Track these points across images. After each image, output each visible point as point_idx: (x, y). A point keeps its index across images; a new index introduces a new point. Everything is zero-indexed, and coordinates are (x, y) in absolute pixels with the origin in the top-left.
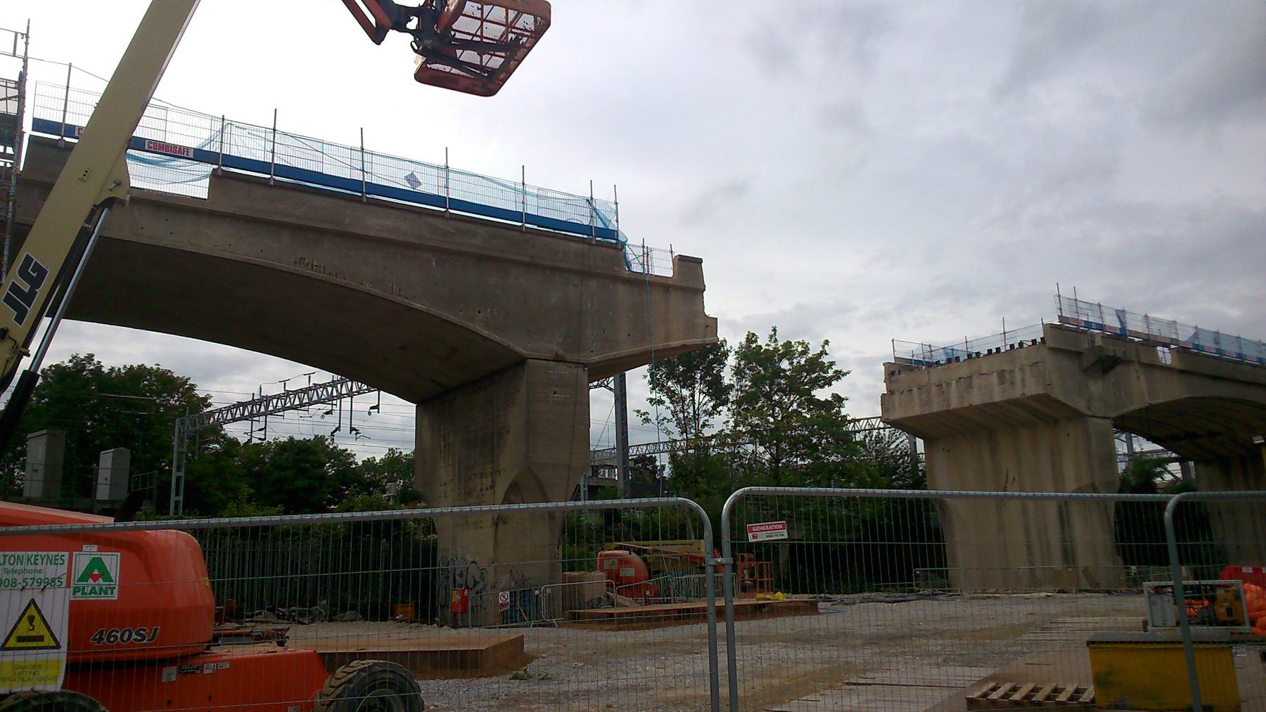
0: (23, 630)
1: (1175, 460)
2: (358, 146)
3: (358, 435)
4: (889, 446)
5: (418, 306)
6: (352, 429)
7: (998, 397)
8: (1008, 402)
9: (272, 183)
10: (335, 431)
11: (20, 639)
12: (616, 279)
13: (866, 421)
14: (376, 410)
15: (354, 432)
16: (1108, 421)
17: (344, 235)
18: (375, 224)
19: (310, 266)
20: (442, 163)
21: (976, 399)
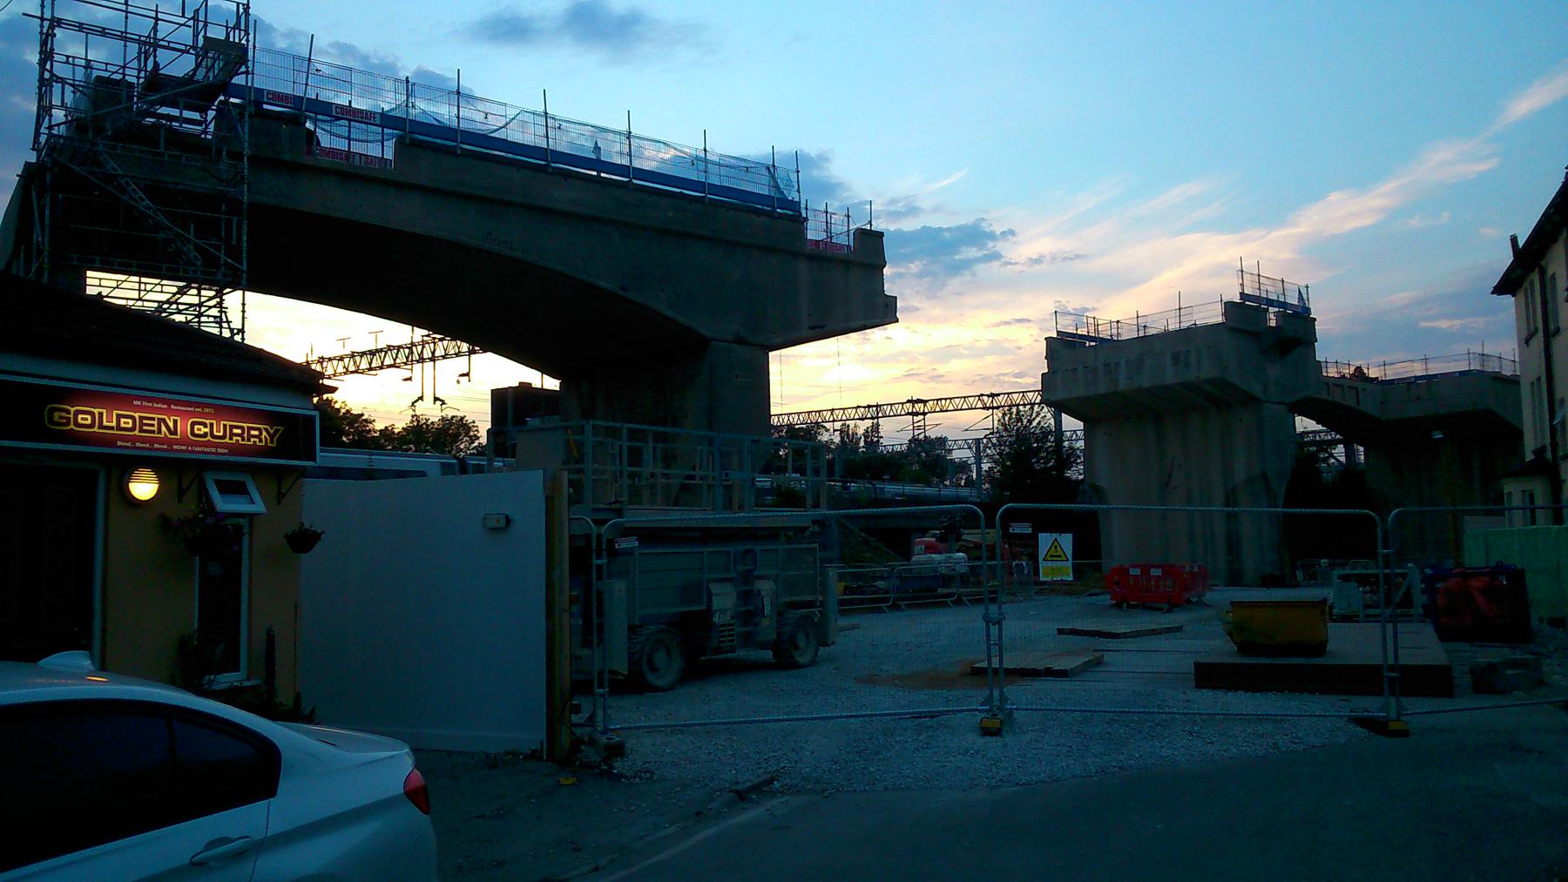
0: (1052, 551)
1: (1340, 442)
2: (541, 109)
3: (444, 406)
4: (1031, 424)
5: (603, 284)
6: (436, 399)
7: (1170, 378)
8: (1186, 385)
9: (459, 152)
10: (416, 401)
11: (1051, 556)
12: (796, 255)
13: (1006, 396)
14: (467, 378)
15: (439, 403)
16: (1283, 407)
17: (531, 208)
18: (561, 197)
19: (497, 241)
20: (624, 128)
21: (1146, 380)
